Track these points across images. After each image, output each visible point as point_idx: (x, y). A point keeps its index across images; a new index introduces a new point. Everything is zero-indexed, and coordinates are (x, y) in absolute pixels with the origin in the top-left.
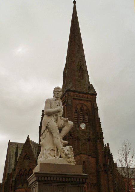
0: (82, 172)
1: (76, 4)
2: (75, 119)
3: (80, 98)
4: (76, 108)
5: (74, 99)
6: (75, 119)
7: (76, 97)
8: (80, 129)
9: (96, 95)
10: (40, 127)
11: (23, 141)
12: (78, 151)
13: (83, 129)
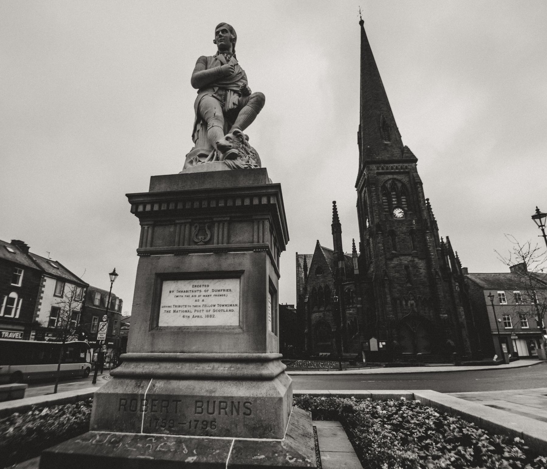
1: (365, 25)
2: (385, 204)
4: (384, 187)
6: (385, 204)
7: (380, 171)
8: (395, 218)
10: (333, 209)
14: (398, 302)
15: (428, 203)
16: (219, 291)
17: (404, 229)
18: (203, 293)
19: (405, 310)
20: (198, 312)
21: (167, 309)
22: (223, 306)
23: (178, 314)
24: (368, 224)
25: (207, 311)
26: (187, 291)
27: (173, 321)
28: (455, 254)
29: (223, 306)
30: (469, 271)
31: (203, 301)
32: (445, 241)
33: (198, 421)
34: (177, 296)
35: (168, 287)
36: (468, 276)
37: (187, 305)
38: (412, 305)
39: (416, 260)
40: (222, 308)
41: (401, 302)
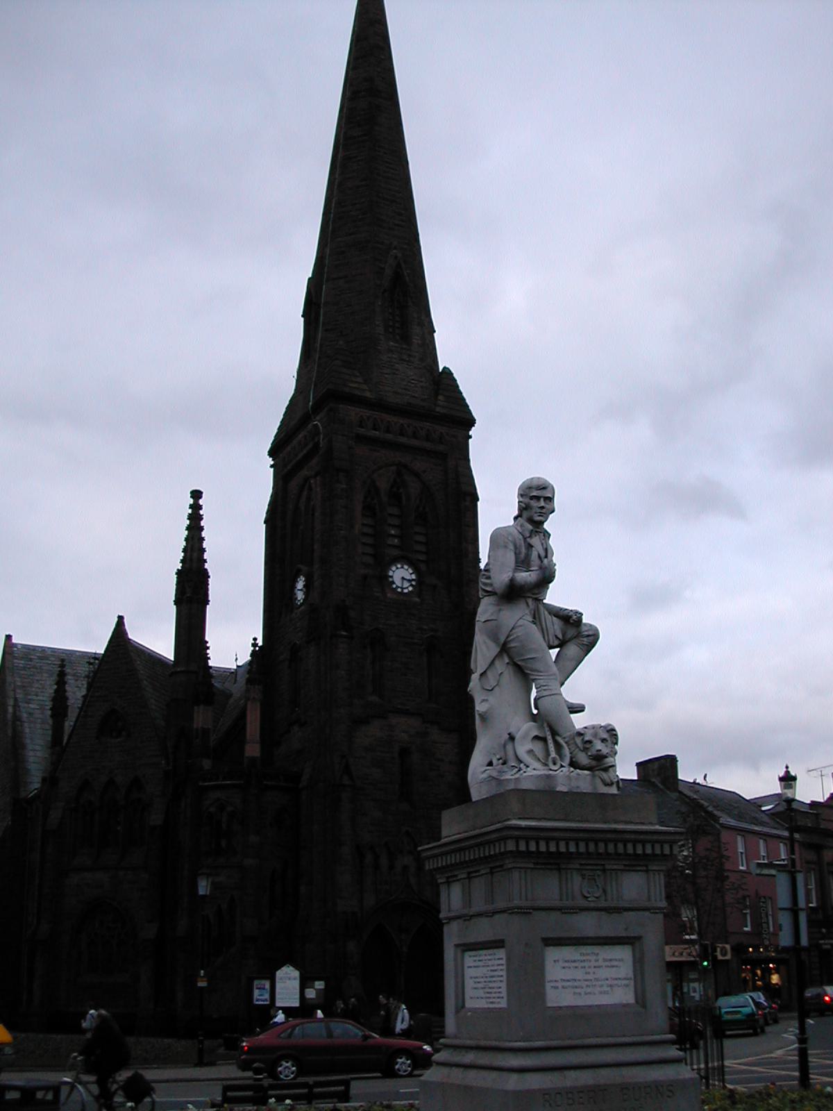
0: (655, 821)
5: (360, 439)
9: (471, 422)
10: (190, 517)
11: (98, 645)
12: (374, 698)
13: (402, 593)
18: (593, 964)
21: (552, 984)
24: (300, 596)
34: (564, 968)
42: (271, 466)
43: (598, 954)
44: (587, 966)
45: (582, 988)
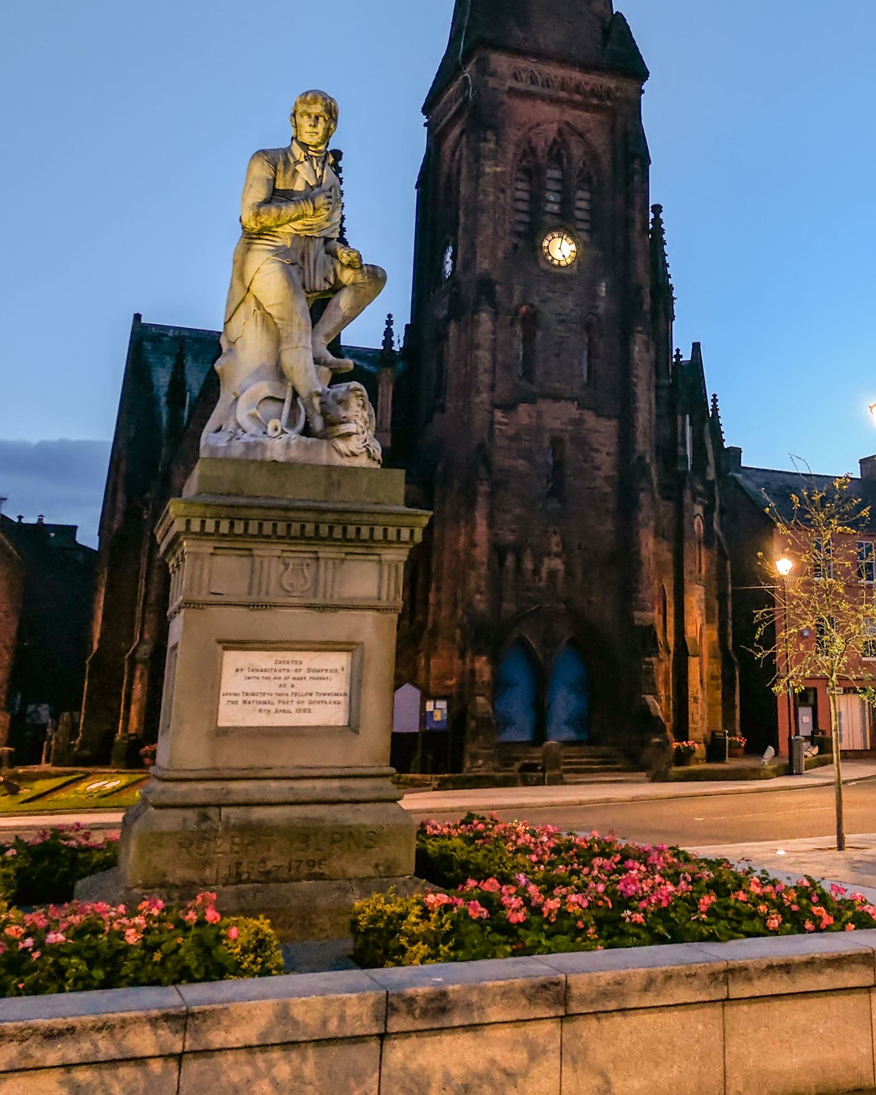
0: (401, 500)
1: (618, 1019)
3: (533, 88)
7: (520, 86)
14: (510, 560)
15: (658, 221)
16: (318, 671)
17: (569, 304)
19: (529, 590)
20: (284, 703)
22: (324, 695)
23: (251, 706)
24: (448, 268)
25: (298, 703)
26: (266, 670)
27: (243, 718)
28: (710, 404)
29: (324, 695)
30: (746, 462)
31: (293, 686)
32: (687, 356)
33: (301, 861)
34: (249, 678)
35: (232, 659)
36: (739, 476)
37: (267, 691)
38: (552, 574)
39: (591, 419)
40: (322, 698)
41: (519, 561)
42: (425, 125)
43: (301, 663)
44: (283, 677)
45: (273, 704)
